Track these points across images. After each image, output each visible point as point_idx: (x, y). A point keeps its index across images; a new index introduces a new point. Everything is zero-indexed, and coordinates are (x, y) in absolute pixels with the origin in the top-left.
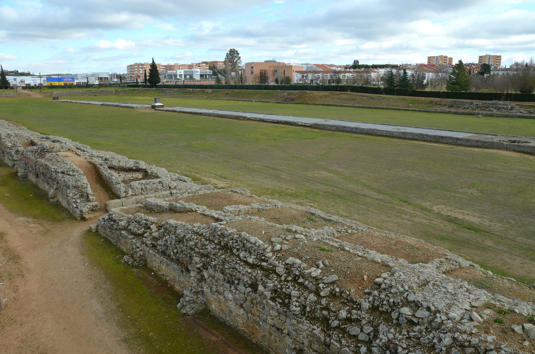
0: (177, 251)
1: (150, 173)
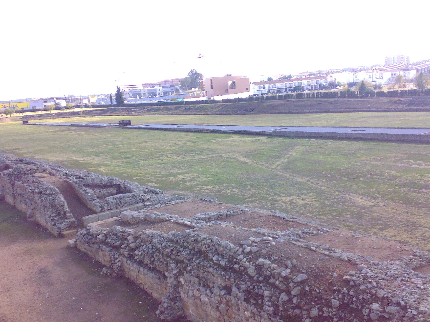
0: (154, 259)
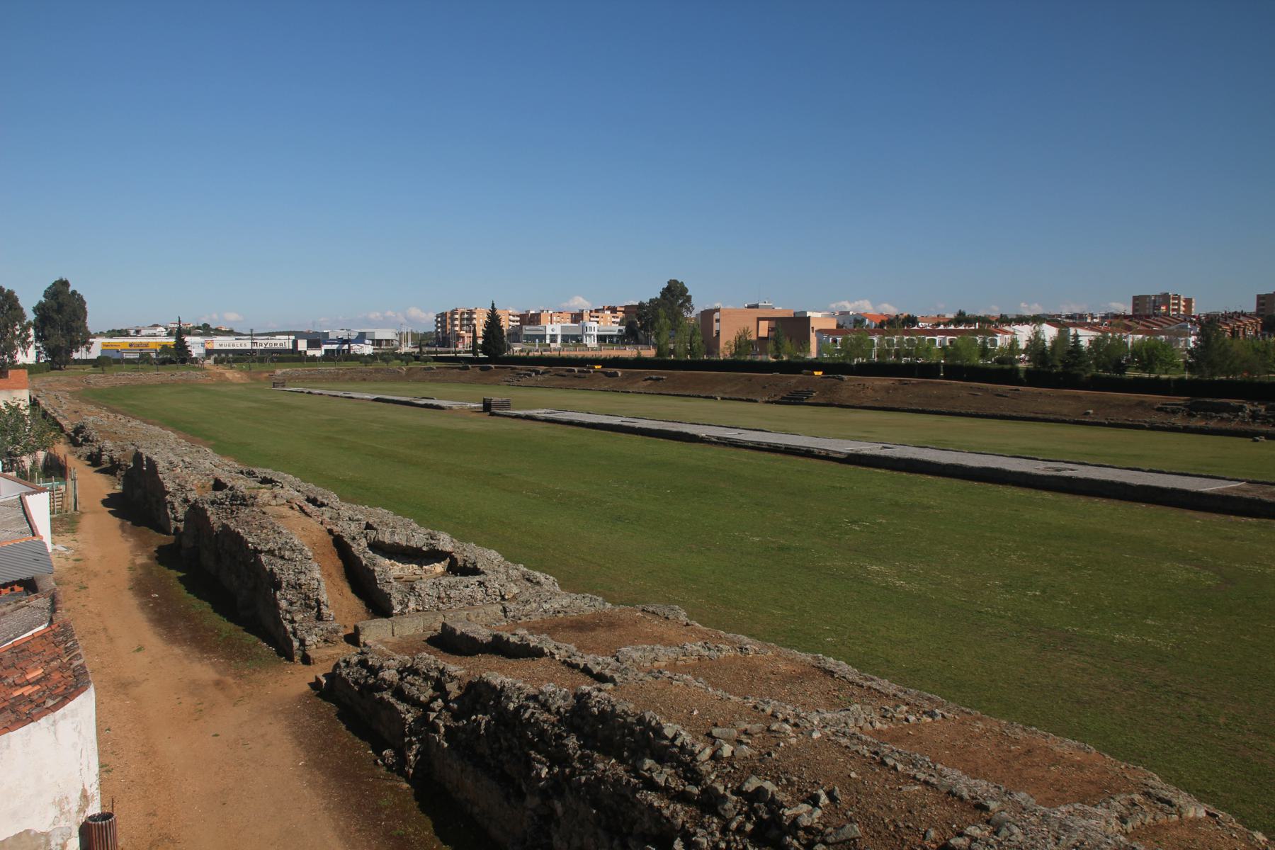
1: (460, 563)
